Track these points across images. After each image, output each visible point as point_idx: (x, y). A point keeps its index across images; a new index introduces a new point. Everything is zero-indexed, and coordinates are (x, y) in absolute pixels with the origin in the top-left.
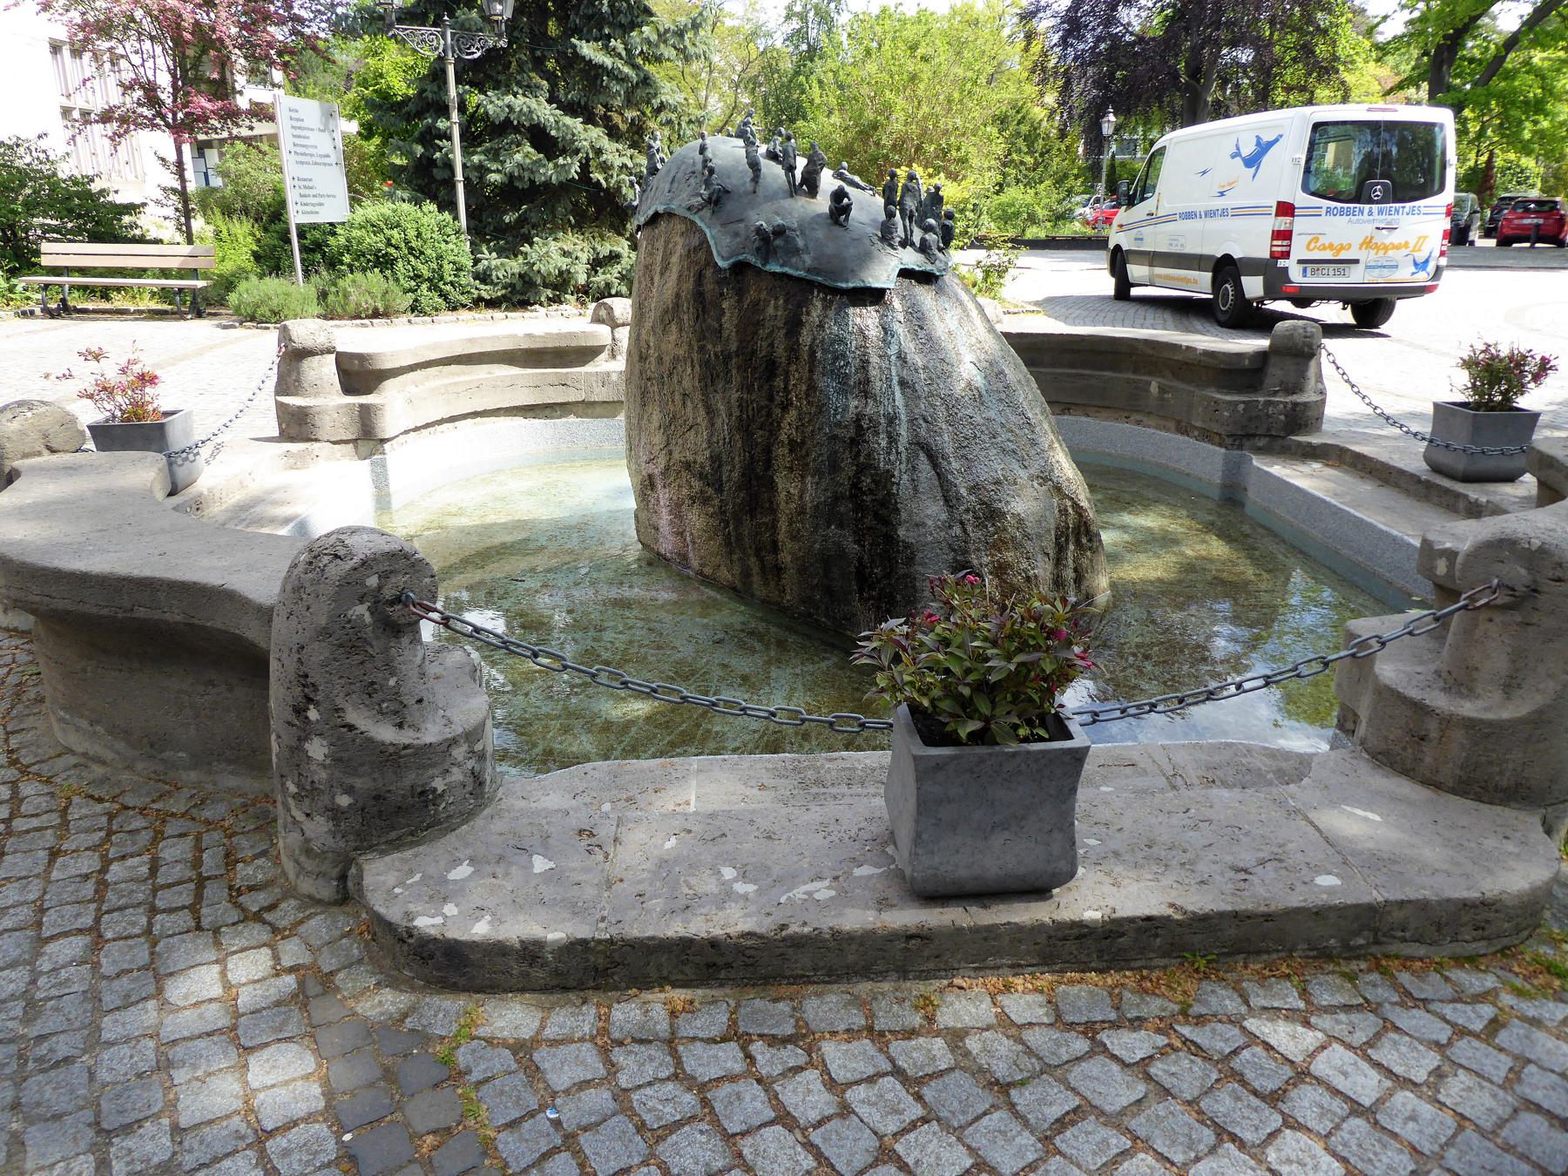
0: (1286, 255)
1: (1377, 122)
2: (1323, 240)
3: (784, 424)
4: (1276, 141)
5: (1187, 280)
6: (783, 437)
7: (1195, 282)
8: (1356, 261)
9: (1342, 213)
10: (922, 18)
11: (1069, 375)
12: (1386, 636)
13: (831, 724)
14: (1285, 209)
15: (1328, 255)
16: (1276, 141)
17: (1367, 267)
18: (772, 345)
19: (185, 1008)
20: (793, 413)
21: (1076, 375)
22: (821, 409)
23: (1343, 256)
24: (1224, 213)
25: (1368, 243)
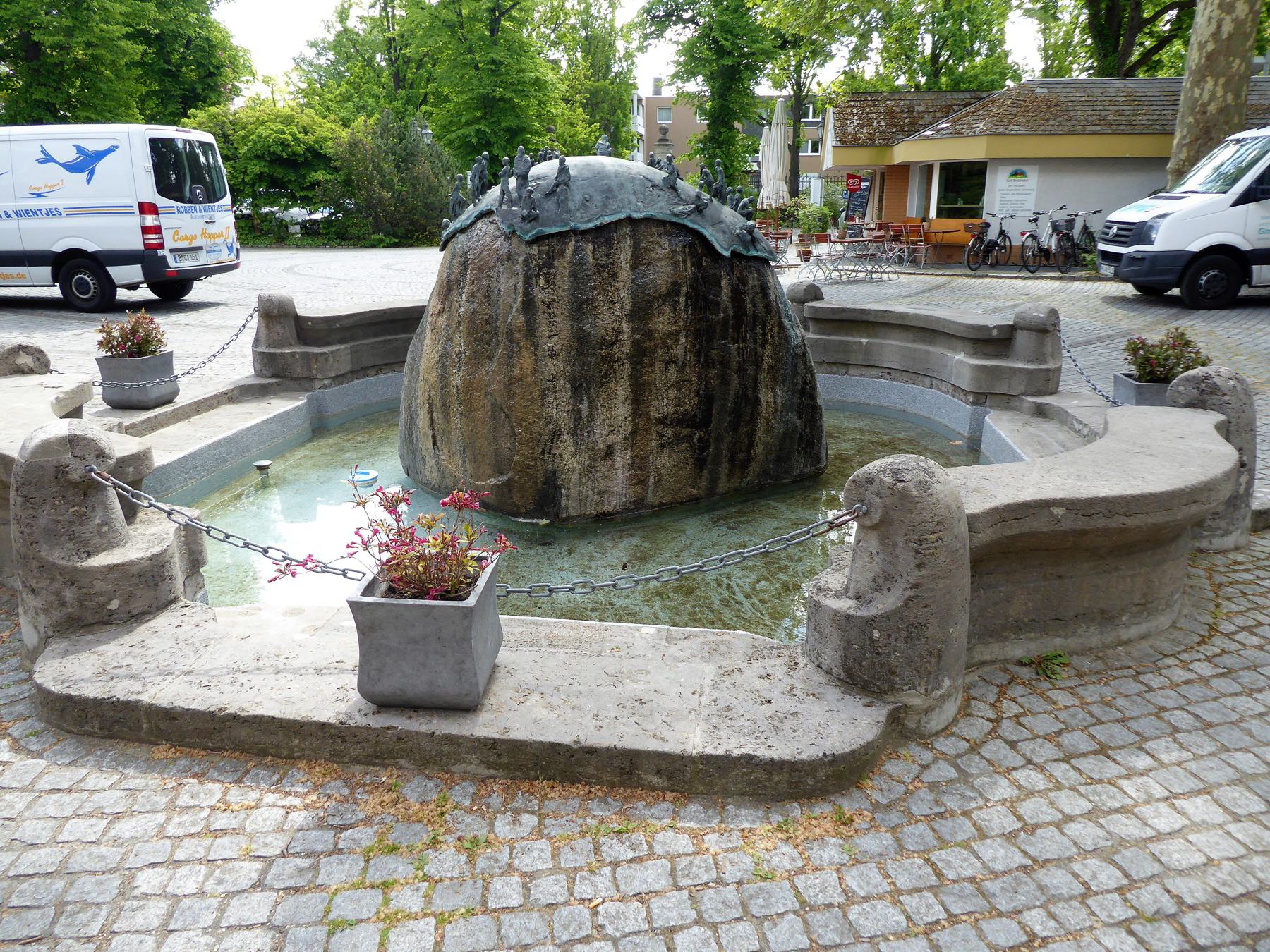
0: (161, 246)
1: (580, 154)
2: (182, 233)
3: (765, 358)
4: (110, 150)
5: (20, 276)
6: (765, 366)
7: (24, 276)
8: (200, 248)
9: (186, 211)
10: (635, 78)
11: (380, 342)
12: (165, 515)
13: (529, 592)
14: (147, 208)
15: (185, 244)
16: (110, 150)
17: (208, 252)
18: (755, 306)
19: (1040, 713)
20: (769, 348)
21: (385, 341)
22: (787, 339)
23: (195, 244)
24: (35, 213)
25: (204, 234)
